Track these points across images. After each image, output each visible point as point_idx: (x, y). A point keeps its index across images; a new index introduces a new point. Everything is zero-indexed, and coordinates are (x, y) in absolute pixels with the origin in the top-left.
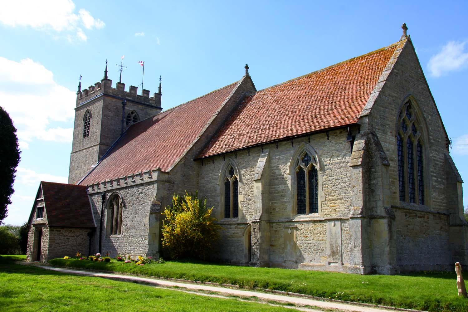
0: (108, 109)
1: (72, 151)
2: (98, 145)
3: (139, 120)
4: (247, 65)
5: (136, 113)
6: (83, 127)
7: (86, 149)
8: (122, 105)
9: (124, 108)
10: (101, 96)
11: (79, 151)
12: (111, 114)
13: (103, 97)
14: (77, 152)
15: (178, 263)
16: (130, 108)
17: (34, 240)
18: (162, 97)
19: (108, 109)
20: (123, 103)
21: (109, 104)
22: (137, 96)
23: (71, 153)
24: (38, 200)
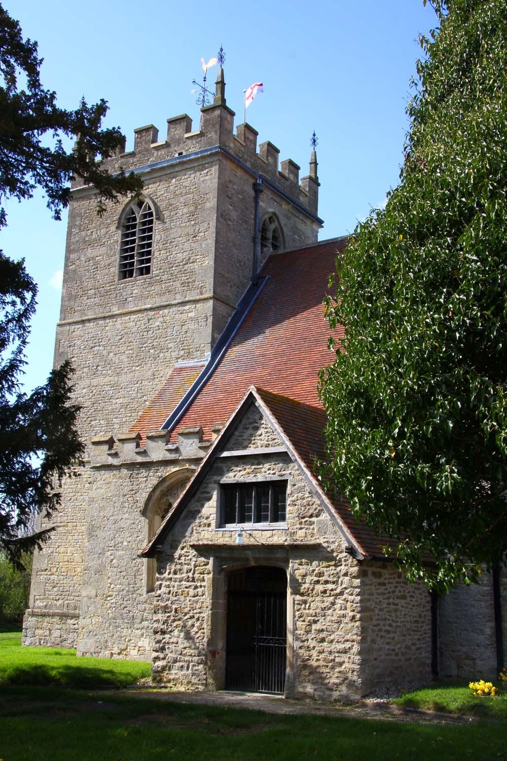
0: (228, 196)
1: (61, 319)
2: (210, 298)
3: (284, 248)
4: (60, 220)
5: (276, 223)
6: (118, 247)
7: (140, 311)
8: (252, 193)
9: (256, 200)
10: (211, 155)
11: (104, 318)
12: (234, 215)
13: (216, 158)
14: (89, 320)
15: (79, 665)
16: (268, 205)
17: (214, 606)
18: (321, 190)
19: (228, 196)
20: (255, 186)
21: (230, 181)
22: (278, 174)
23: (59, 325)
24: (226, 454)
